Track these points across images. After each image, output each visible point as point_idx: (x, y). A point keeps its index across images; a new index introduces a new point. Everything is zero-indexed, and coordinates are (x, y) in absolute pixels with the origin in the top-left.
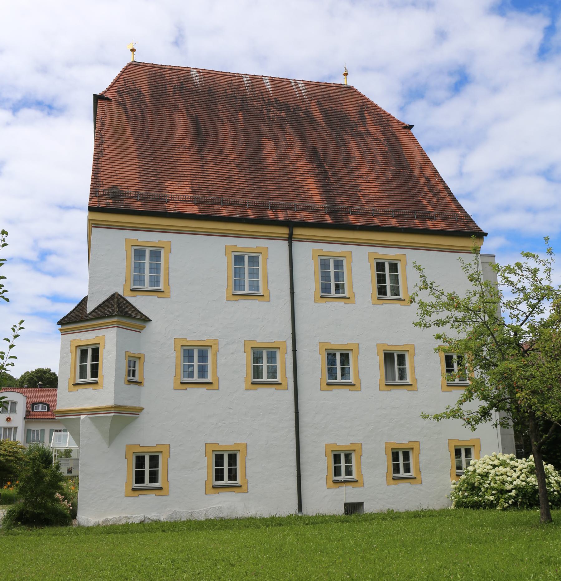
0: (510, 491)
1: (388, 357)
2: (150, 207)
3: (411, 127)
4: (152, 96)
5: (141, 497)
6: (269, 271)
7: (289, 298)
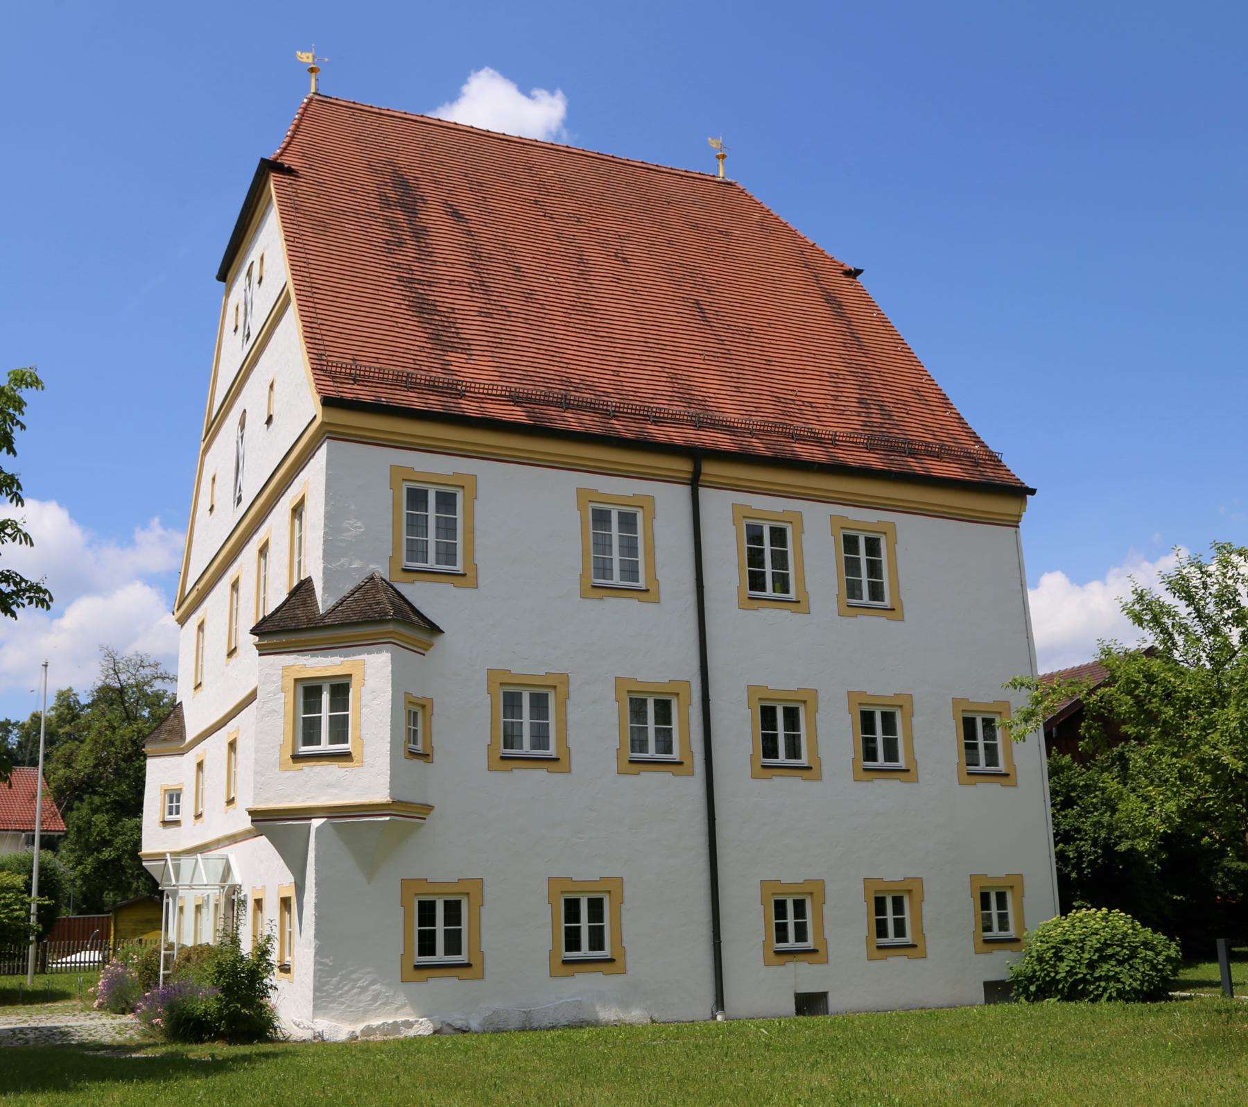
2: (434, 403)
3: (858, 272)
6: (657, 543)
7: (692, 598)
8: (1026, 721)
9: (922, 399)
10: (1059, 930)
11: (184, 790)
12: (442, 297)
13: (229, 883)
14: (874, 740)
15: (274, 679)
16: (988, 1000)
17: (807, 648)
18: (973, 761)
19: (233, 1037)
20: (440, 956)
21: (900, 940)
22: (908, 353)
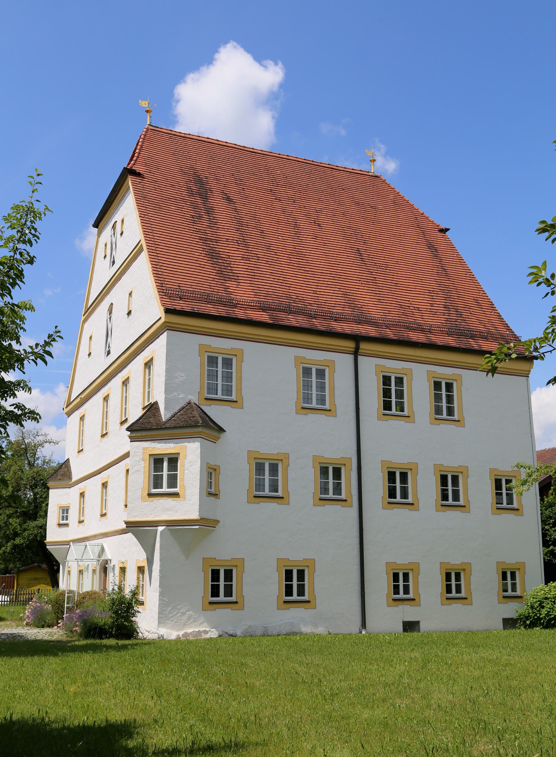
2: (221, 311)
3: (447, 230)
6: (336, 386)
8: (523, 485)
9: (479, 304)
10: (543, 592)
11: (71, 507)
12: (224, 249)
13: (103, 558)
14: (447, 490)
15: (138, 454)
16: (505, 628)
17: (412, 441)
19: (118, 637)
21: (458, 595)
22: (472, 277)
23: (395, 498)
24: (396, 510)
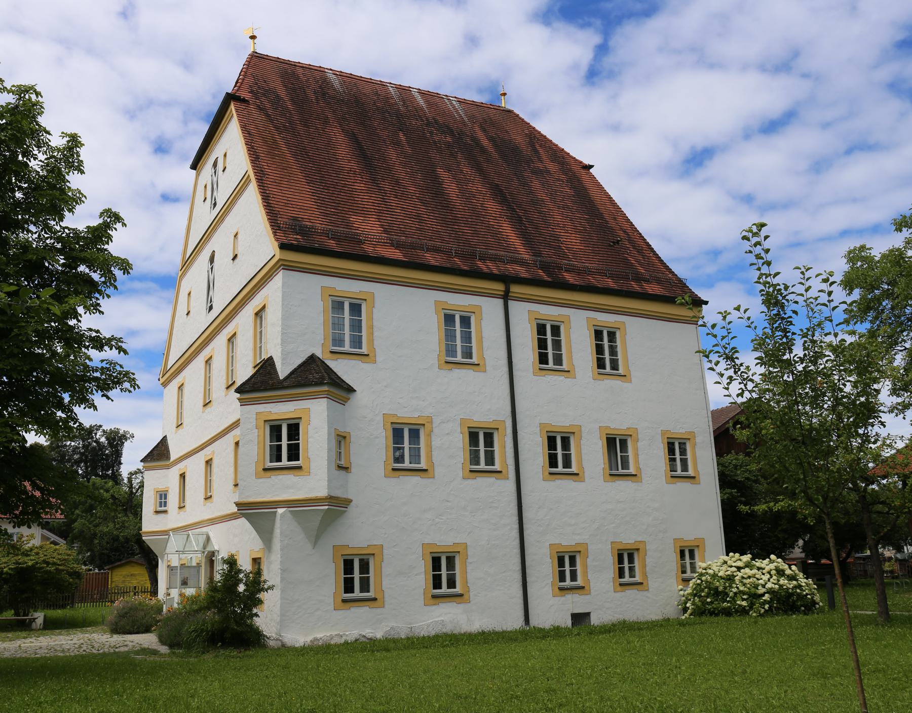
0: (763, 595)
1: (611, 442)
4: (292, 100)
5: (353, 609)
6: (484, 335)
7: (506, 369)
11: (170, 491)
17: (574, 399)
18: (673, 469)
20: (357, 594)
23: (547, 364)
24: (558, 482)
